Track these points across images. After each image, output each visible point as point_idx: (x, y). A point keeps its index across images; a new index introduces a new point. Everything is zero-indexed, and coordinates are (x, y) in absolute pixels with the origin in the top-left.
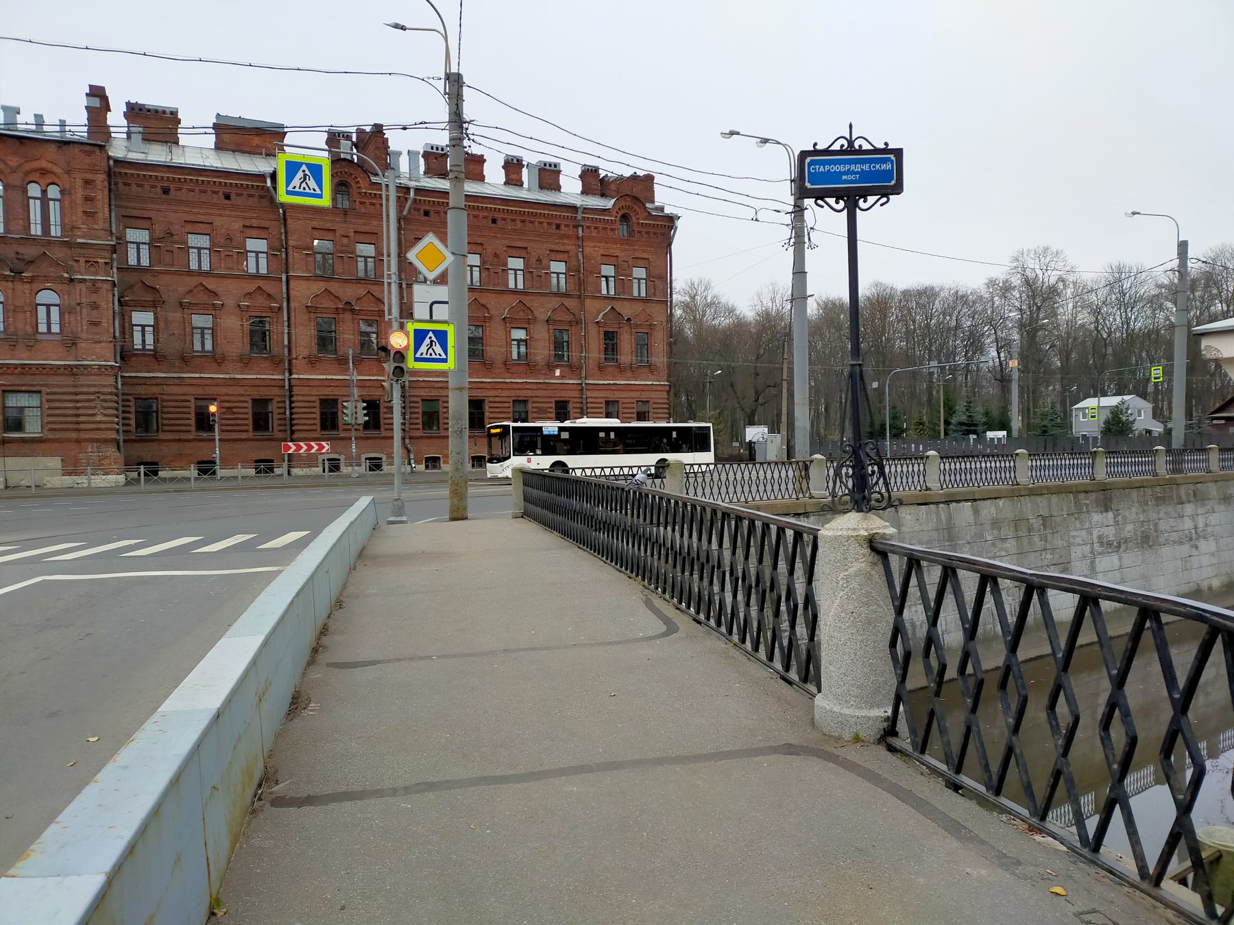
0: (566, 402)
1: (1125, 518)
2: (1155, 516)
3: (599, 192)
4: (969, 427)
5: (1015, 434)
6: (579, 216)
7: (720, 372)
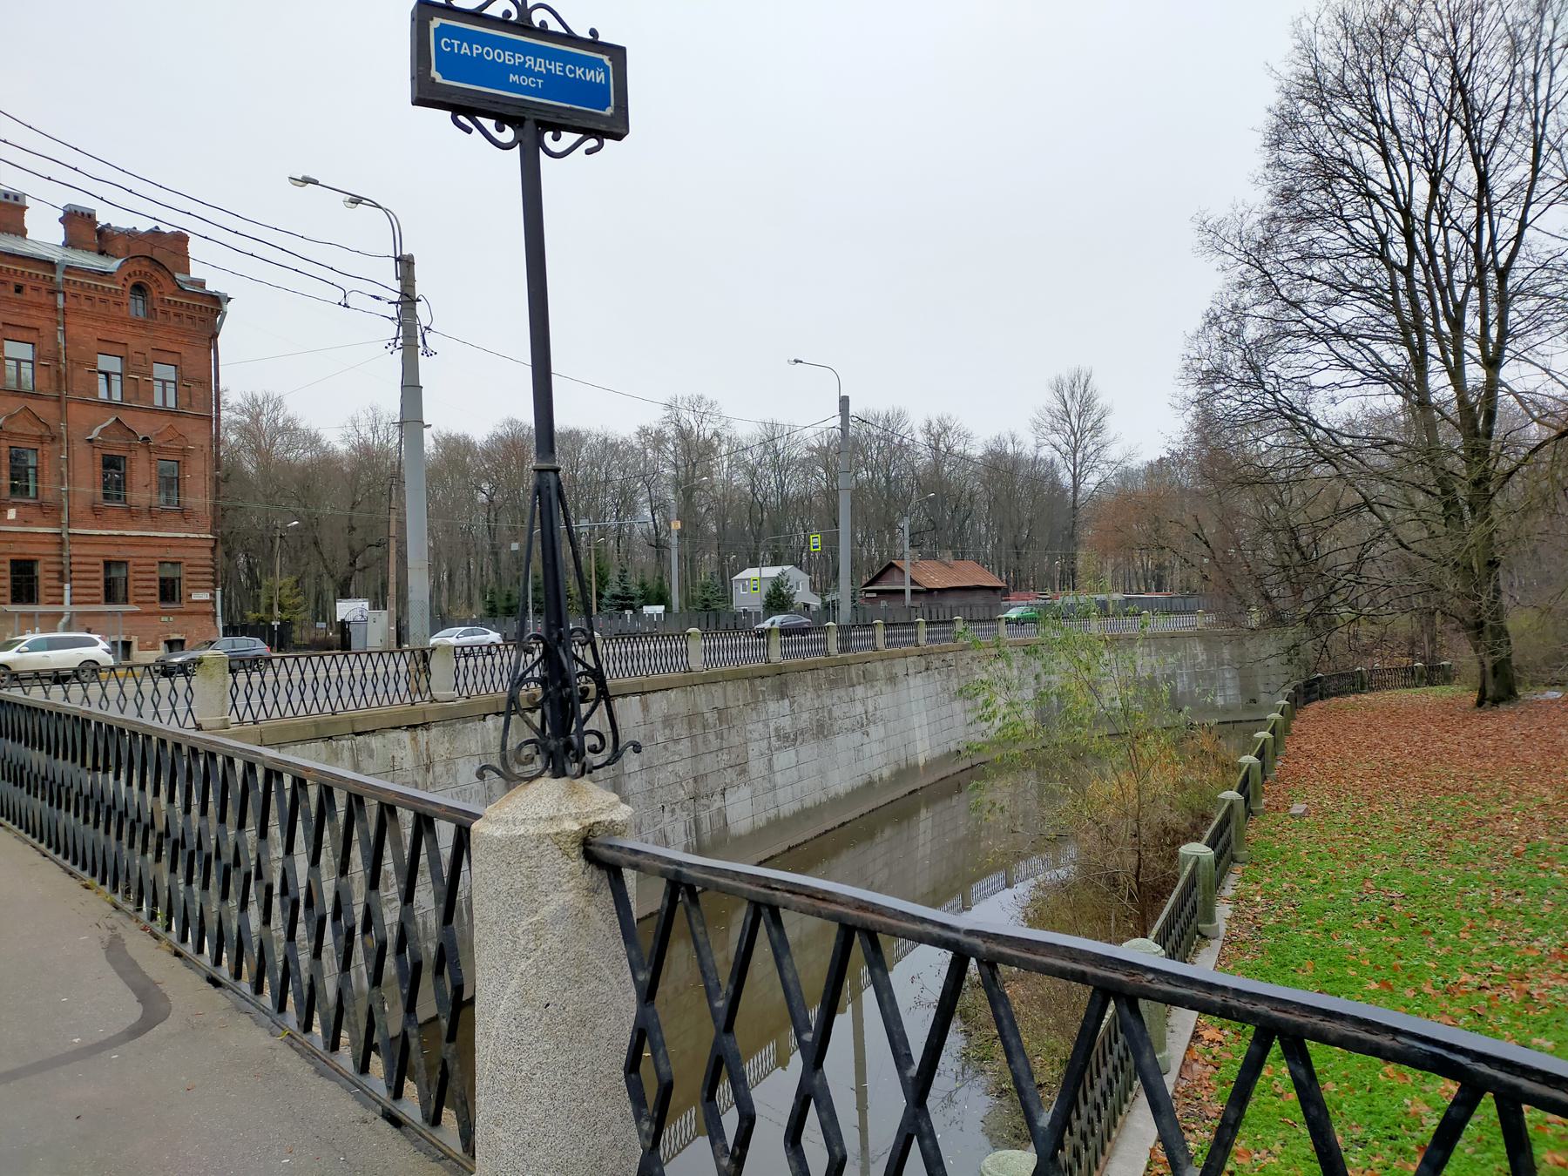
0: (32, 562)
1: (800, 706)
2: (828, 702)
3: (96, 248)
4: (625, 602)
5: (675, 608)
6: (59, 276)
7: (296, 523)
